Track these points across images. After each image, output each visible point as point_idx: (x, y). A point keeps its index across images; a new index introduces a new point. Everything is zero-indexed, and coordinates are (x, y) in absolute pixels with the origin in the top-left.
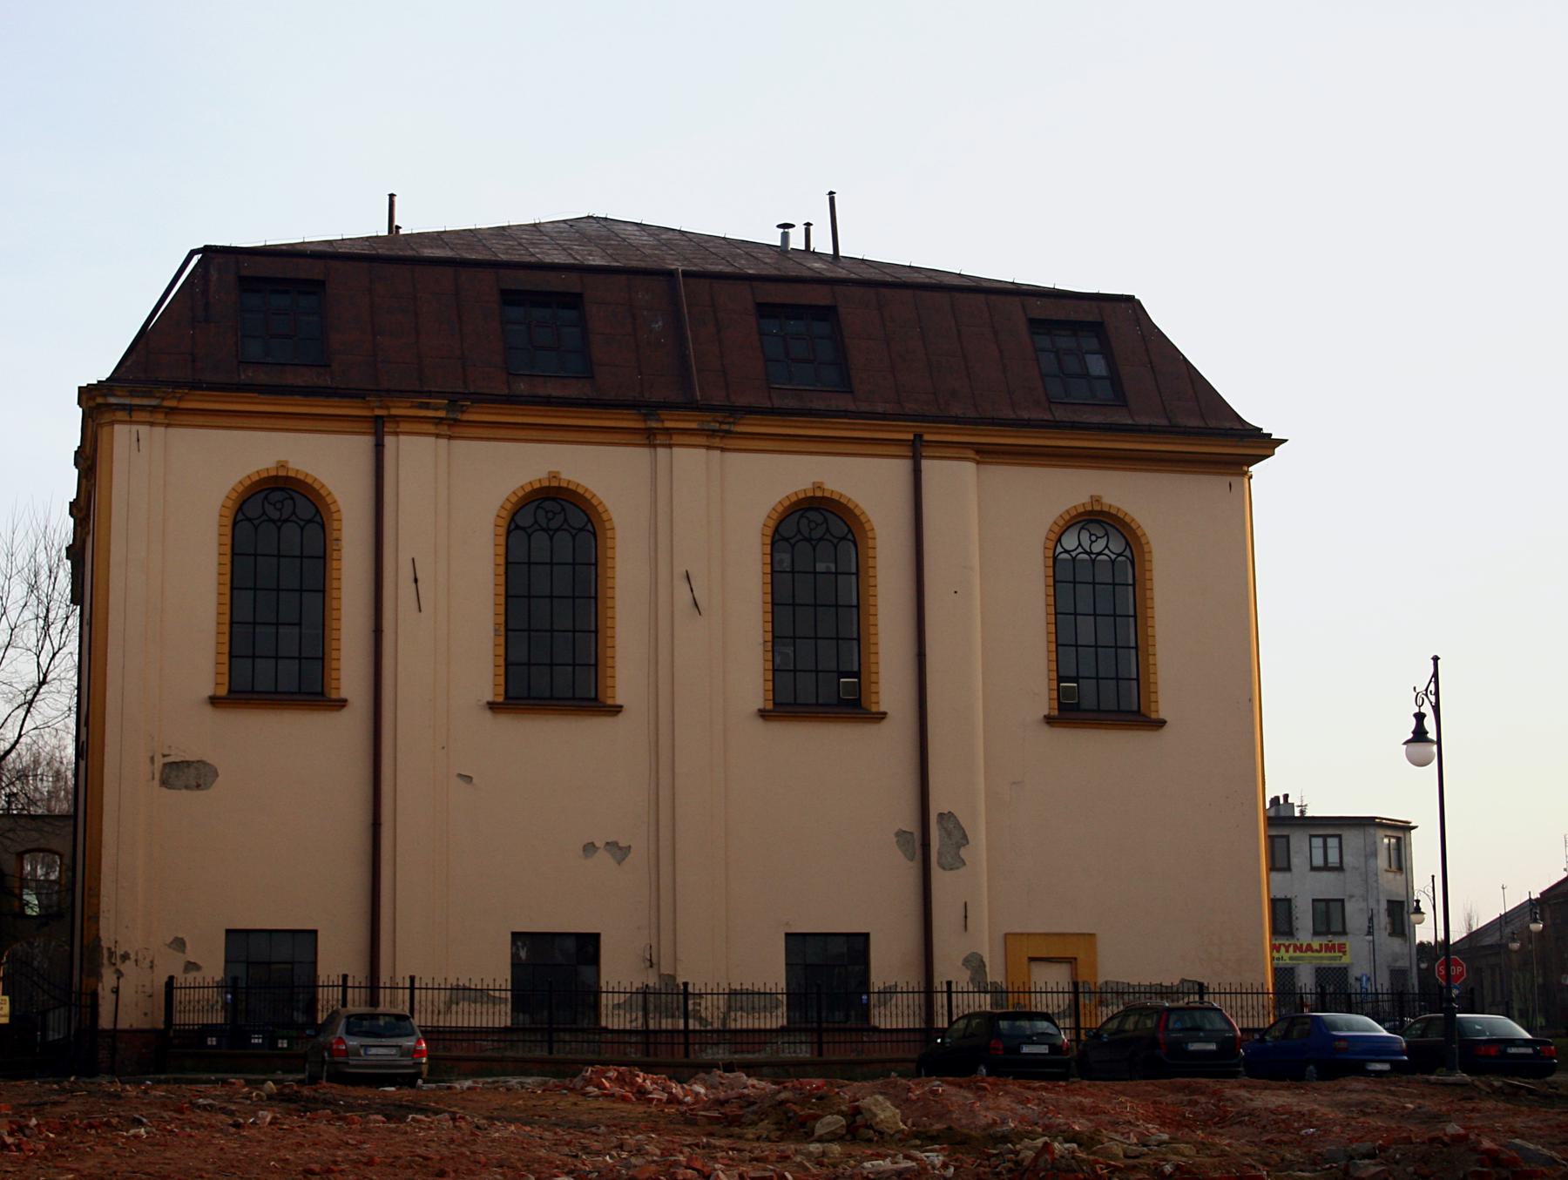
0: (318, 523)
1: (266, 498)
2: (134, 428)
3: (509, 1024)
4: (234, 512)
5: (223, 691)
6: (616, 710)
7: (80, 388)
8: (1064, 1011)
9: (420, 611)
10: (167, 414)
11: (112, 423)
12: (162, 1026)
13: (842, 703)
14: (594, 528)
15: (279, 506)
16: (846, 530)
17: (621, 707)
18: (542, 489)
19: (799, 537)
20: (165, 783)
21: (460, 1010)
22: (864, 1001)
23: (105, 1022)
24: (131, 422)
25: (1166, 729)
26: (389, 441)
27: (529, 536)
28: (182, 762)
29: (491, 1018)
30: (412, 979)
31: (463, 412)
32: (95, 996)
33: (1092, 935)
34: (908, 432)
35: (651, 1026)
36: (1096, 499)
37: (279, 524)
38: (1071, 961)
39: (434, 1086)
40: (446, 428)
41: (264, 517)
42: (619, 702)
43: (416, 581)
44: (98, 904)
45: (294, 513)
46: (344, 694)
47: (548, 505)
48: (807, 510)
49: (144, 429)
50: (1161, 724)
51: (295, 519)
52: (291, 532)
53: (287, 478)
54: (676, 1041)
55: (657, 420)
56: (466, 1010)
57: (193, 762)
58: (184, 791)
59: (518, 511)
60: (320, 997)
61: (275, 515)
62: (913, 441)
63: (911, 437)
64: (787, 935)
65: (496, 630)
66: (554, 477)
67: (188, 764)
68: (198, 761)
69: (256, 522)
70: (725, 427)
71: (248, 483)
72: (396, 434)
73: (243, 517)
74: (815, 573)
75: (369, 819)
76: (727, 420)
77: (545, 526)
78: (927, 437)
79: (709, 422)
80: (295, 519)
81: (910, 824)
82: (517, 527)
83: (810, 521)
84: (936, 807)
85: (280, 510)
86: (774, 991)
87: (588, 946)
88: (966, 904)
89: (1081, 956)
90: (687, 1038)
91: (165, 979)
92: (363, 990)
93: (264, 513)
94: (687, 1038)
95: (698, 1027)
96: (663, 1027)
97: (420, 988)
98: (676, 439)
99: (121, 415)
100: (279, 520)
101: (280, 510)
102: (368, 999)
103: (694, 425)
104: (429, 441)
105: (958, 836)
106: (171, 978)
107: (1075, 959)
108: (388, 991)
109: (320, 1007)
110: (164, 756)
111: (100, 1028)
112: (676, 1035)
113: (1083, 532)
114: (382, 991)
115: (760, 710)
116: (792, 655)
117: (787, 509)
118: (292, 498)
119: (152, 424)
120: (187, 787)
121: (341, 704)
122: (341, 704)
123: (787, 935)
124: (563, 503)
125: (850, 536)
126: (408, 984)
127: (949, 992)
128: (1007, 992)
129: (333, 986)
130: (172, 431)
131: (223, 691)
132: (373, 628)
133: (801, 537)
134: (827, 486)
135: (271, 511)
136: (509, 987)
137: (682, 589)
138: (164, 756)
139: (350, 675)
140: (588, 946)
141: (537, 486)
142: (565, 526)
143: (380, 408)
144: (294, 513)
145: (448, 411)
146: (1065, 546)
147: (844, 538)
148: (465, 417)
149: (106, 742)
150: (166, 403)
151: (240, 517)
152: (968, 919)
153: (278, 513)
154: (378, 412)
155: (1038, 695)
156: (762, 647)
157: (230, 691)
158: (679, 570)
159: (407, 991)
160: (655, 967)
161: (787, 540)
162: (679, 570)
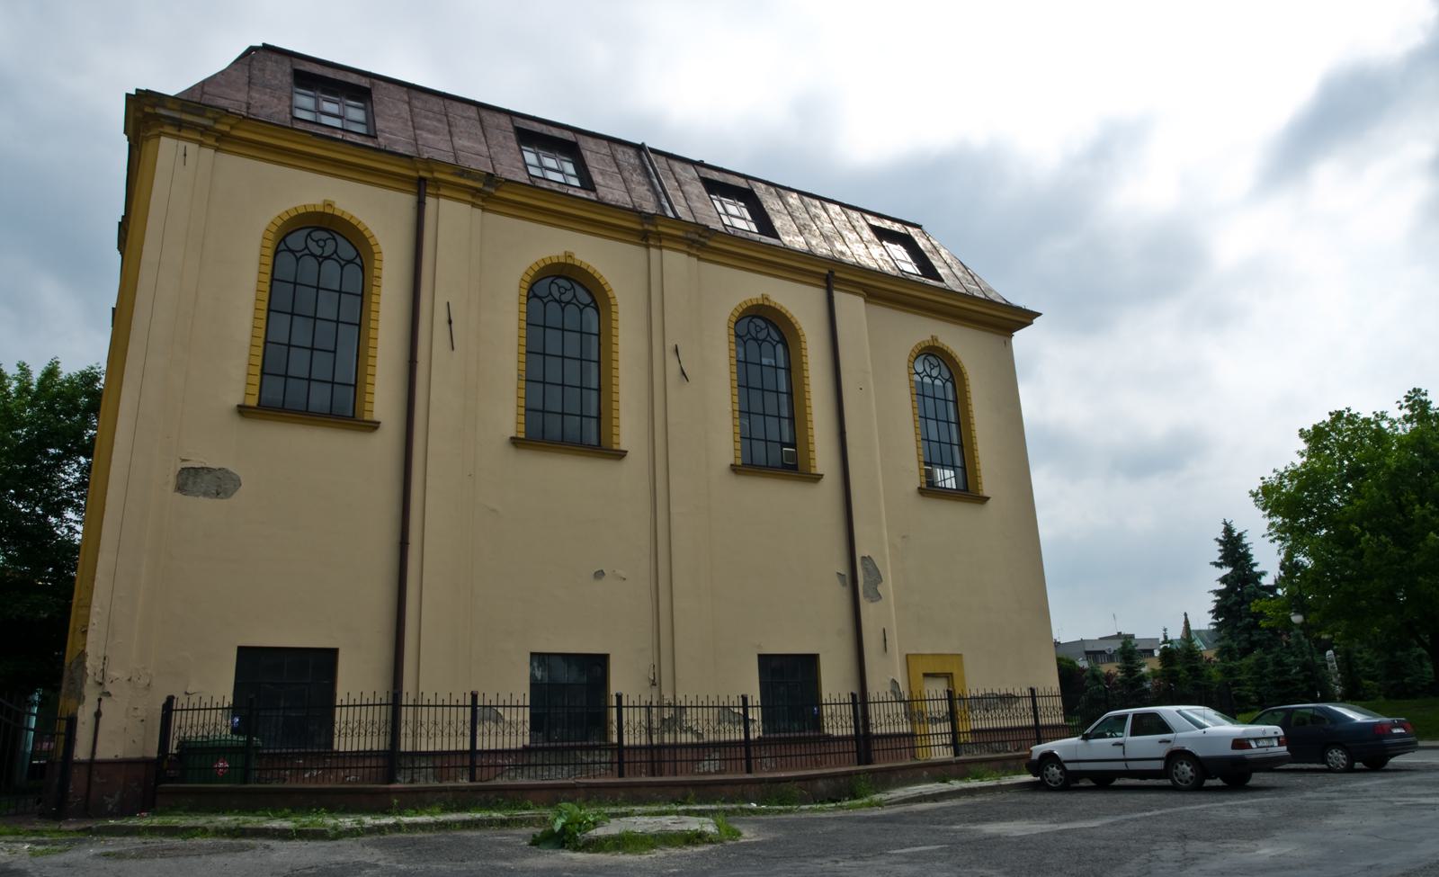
0: (284, 250)
1: (309, 234)
2: (182, 144)
3: (527, 741)
4: (278, 241)
5: (253, 402)
6: (620, 455)
7: (128, 96)
8: (943, 717)
9: (453, 348)
10: (217, 140)
11: (158, 136)
12: (155, 755)
13: (785, 467)
14: (362, 262)
15: (322, 243)
16: (354, 254)
17: (379, 423)
18: (559, 264)
19: (550, 298)
20: (181, 488)
21: (486, 731)
22: (816, 713)
23: (81, 752)
24: (178, 138)
25: (989, 502)
26: (430, 202)
27: (545, 305)
28: (203, 468)
29: (507, 739)
30: (474, 696)
31: (497, 189)
32: (72, 722)
33: (960, 655)
34: (826, 268)
35: (655, 741)
36: (765, 298)
37: (321, 259)
38: (948, 676)
39: (833, 805)
40: (480, 200)
41: (306, 251)
42: (623, 447)
43: (450, 322)
44: (88, 617)
45: (335, 252)
46: (376, 416)
47: (562, 282)
48: (754, 317)
49: (192, 148)
50: (985, 499)
51: (337, 258)
52: (330, 267)
53: (333, 216)
54: (678, 758)
55: (652, 225)
56: (493, 731)
57: (214, 469)
58: (201, 498)
59: (535, 283)
60: (337, 719)
61: (318, 251)
62: (827, 276)
63: (826, 272)
64: (760, 656)
65: (519, 375)
66: (570, 256)
67: (209, 470)
68: (220, 469)
69: (298, 255)
70: (702, 240)
71: (286, 217)
72: (437, 196)
73: (335, 255)
74: (761, 365)
75: (395, 538)
76: (704, 234)
77: (558, 298)
78: (837, 274)
79: (691, 233)
80: (337, 258)
81: (842, 568)
82: (535, 296)
83: (559, 288)
84: (861, 552)
85: (322, 247)
86: (494, 703)
87: (596, 666)
88: (884, 630)
89: (955, 672)
90: (748, 752)
91: (164, 701)
92: (384, 708)
93: (307, 247)
94: (748, 752)
95: (695, 740)
96: (666, 741)
97: (524, 706)
98: (665, 243)
99: (168, 129)
100: (320, 256)
101: (322, 247)
102: (389, 718)
103: (680, 233)
104: (684, 256)
105: (875, 576)
106: (170, 699)
107: (951, 674)
108: (411, 709)
109: (336, 732)
110: (184, 460)
111: (75, 758)
112: (678, 751)
113: (751, 324)
114: (404, 709)
115: (512, 438)
116: (748, 426)
117: (537, 273)
118: (334, 239)
119: (201, 144)
120: (205, 494)
121: (373, 426)
122: (373, 426)
123: (760, 656)
124: (335, 234)
125: (358, 261)
126: (469, 702)
127: (620, 707)
128: (896, 701)
129: (354, 706)
130: (221, 155)
131: (253, 402)
132: (408, 359)
133: (297, 254)
134: (337, 205)
135: (312, 245)
136: (528, 703)
137: (672, 359)
138: (184, 460)
139: (383, 399)
140: (596, 666)
141: (555, 261)
142: (335, 256)
143: (425, 170)
144: (335, 252)
145: (484, 185)
146: (572, 306)
147: (587, 305)
148: (499, 194)
149: (116, 440)
150: (218, 127)
151: (282, 247)
152: (887, 642)
153: (320, 249)
154: (423, 174)
155: (507, 417)
156: (731, 414)
157: (259, 404)
158: (670, 345)
159: (468, 710)
160: (658, 686)
161: (540, 298)
162: (670, 345)
